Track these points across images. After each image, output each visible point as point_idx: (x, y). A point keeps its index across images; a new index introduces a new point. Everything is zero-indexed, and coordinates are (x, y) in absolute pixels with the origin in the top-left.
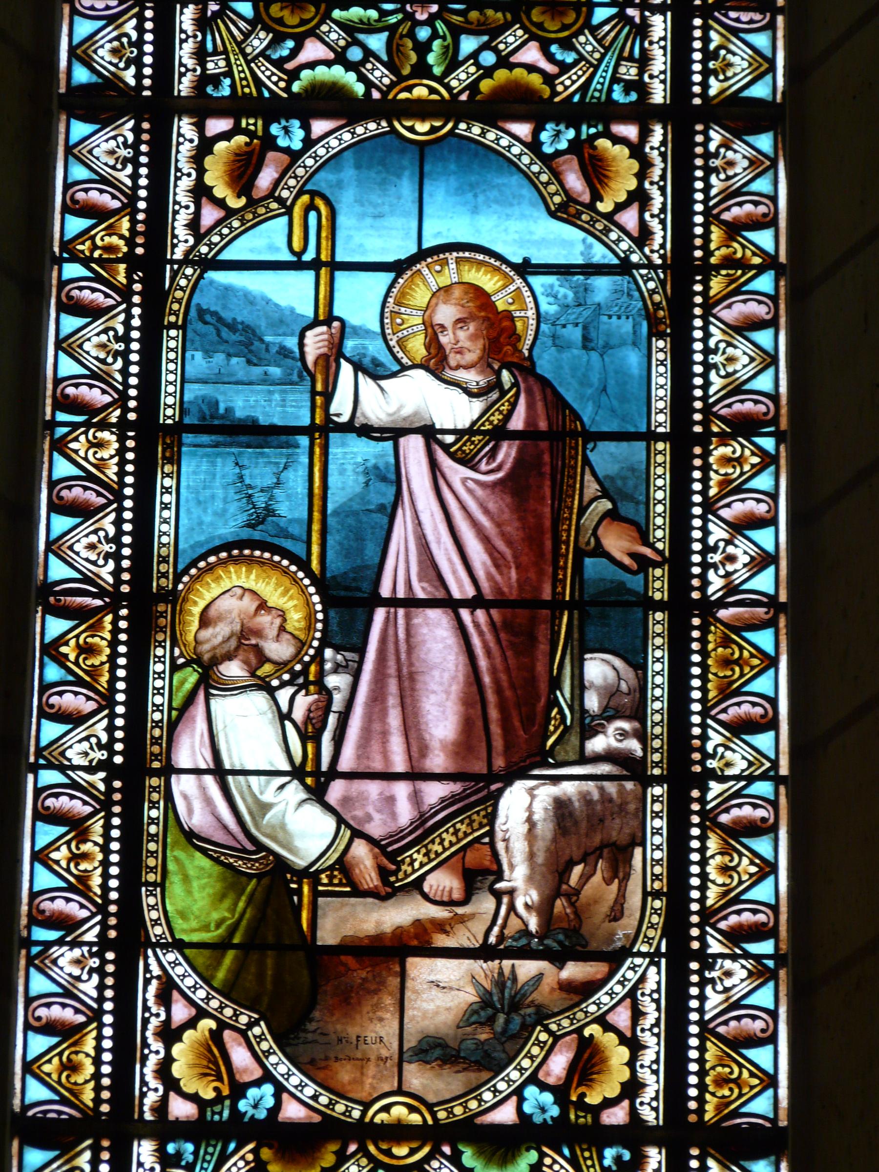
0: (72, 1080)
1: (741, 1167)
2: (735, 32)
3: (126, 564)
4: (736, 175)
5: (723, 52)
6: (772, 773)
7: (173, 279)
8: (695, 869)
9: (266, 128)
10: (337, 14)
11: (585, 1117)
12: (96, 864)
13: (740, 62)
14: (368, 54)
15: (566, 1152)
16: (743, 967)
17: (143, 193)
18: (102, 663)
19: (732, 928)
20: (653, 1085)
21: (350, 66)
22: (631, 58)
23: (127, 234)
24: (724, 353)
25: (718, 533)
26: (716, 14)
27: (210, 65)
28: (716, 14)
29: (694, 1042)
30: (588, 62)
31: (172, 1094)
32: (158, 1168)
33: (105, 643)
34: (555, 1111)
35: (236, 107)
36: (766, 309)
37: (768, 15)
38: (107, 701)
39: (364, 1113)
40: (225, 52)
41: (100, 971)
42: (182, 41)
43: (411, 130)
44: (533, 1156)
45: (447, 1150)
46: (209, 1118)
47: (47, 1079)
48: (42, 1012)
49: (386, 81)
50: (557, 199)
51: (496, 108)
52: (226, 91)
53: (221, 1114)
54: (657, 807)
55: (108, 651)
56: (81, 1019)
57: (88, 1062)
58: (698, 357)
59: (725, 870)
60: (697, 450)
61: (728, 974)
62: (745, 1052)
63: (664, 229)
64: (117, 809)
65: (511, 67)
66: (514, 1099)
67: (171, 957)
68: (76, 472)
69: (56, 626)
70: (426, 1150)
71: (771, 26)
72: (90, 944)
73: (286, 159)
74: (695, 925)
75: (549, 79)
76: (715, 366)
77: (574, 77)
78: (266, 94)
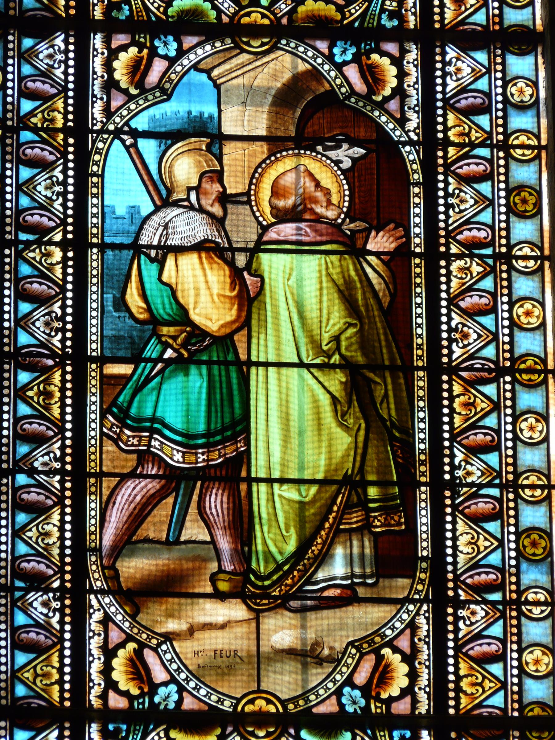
0: (46, 542)
3: (69, 335)
4: (469, 344)
6: (489, 142)
7: (94, 142)
8: (449, 543)
11: (381, 708)
16: (482, 609)
18: (54, 543)
19: (466, 240)
20: (97, 64)
24: (455, 65)
29: (444, 311)
35: (390, 722)
38: (60, 502)
42: (90, 638)
45: (292, 731)
49: (232, 10)
50: (164, 647)
53: (143, 703)
54: (418, 280)
55: (58, 534)
56: (54, 91)
57: (54, 671)
59: (466, 405)
61: (473, 613)
62: (487, 667)
64: (70, 263)
67: (107, 600)
68: (35, 342)
69: (24, 377)
70: (239, 708)
72: (54, 591)
73: (166, 64)
76: (450, 74)
77: (357, 8)
78: (154, 19)
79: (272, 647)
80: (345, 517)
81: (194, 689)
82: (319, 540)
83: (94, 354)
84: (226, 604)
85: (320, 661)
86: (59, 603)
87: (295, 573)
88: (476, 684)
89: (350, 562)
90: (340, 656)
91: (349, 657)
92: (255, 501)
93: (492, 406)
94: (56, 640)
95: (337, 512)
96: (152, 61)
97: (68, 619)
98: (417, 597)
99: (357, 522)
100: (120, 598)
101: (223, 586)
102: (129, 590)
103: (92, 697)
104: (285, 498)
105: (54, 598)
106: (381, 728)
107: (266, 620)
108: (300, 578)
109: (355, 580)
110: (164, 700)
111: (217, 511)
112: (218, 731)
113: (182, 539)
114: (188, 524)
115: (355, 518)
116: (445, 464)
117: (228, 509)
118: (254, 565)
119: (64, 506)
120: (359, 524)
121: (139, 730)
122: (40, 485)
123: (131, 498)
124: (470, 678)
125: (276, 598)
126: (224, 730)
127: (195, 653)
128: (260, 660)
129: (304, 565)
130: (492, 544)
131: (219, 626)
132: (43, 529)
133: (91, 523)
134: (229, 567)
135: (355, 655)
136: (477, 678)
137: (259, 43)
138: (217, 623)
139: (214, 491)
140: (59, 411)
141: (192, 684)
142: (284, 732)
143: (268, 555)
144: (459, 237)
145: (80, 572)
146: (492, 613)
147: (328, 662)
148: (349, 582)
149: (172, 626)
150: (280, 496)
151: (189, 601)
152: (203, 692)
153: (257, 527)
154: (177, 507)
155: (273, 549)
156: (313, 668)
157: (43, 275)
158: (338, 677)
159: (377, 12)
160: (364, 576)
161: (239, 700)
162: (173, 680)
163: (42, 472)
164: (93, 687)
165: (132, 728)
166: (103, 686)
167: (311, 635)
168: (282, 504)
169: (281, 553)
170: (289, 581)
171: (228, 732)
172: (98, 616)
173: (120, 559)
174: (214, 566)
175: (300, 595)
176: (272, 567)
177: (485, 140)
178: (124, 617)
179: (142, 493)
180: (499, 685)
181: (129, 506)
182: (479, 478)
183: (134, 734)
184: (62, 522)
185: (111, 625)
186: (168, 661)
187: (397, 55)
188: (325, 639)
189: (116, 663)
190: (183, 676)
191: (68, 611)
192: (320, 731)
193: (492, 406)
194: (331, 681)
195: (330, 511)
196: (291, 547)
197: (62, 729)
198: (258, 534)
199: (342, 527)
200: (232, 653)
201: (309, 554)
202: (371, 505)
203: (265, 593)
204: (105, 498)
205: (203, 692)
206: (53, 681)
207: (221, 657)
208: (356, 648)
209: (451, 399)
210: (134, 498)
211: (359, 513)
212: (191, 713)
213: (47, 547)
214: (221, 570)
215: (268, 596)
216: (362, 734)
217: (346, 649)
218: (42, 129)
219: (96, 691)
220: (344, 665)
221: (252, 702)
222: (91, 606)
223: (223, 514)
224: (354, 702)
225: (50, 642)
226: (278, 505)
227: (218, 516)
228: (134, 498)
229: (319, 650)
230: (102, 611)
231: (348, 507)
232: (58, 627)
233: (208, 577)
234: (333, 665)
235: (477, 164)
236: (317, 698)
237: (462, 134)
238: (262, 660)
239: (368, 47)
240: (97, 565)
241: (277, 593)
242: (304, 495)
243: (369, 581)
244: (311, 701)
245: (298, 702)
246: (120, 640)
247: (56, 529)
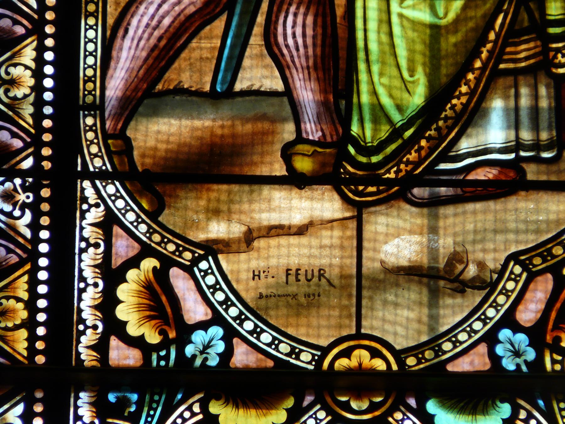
0: (11, 94)
15: (541, 403)
17: (44, 248)
18: (26, 96)
32: (97, 421)
33: (21, 305)
34: (531, 355)
38: (36, 28)
41: (34, 207)
42: (82, 251)
44: (506, 410)
45: (412, 402)
46: (155, 363)
50: (204, 265)
53: (167, 358)
67: (111, 189)
72: (23, 174)
79: (382, 262)
80: (508, 49)
81: (251, 333)
82: (464, 89)
84: (306, 192)
85: (461, 286)
86: (31, 195)
87: (423, 143)
89: (515, 122)
90: (495, 276)
91: (509, 279)
92: (359, 23)
94: (24, 256)
95: (495, 42)
96: (159, 222)
97: (45, 221)
99: (526, 58)
100: (131, 184)
101: (303, 165)
102: (146, 171)
103: (81, 349)
104: (408, 19)
105: (22, 186)
106: (560, 397)
107: (372, 218)
108: (431, 150)
109: (523, 154)
110: (202, 352)
111: (296, 43)
112: (290, 403)
113: (238, 87)
114: (246, 62)
115: (524, 51)
117: (314, 37)
118: (355, 129)
119: (43, 36)
120: (532, 61)
121: (158, 402)
123: (154, 23)
125: (390, 183)
126: (299, 401)
127: (256, 276)
128: (362, 284)
129: (438, 129)
131: (293, 230)
132: (7, 73)
133: (88, 64)
134: (315, 136)
135: (520, 275)
137: (365, 405)
138: (293, 224)
139: (292, 9)
141: (249, 325)
142: (399, 404)
143: (379, 113)
145: (68, 142)
147: (474, 288)
148: (512, 156)
149: (217, 230)
150: (401, 16)
151: (246, 188)
152: (266, 338)
153: (362, 66)
154: (231, 34)
155: (386, 100)
156: (450, 296)
158: (491, 312)
160: (537, 146)
161: (325, 351)
162: (217, 319)
164: (83, 333)
165: (147, 397)
166: (100, 330)
167: (446, 244)
168: (402, 26)
169: (400, 108)
170: (413, 156)
171: (305, 403)
172: (95, 215)
173: (132, 123)
174: (288, 132)
175: (431, 177)
176: (385, 131)
178: (138, 216)
179: (173, 14)
181: (151, 35)
183: (150, 408)
184: (40, 61)
185: (116, 230)
186: (209, 287)
188: (469, 248)
189: (124, 292)
190: (233, 312)
191: (45, 207)
192: (459, 402)
194: (479, 319)
195: (483, 41)
196: (418, 98)
197: (29, 403)
198: (363, 77)
199: (502, 66)
200: (316, 273)
201: (448, 108)
202: (552, 30)
203: (372, 175)
204: (110, 21)
205: (266, 338)
206: (18, 322)
207: (298, 280)
208: (522, 264)
210: (160, 22)
211: (532, 45)
212: (246, 372)
214: (300, 139)
215: (377, 181)
216: (528, 407)
217: (505, 266)
219: (89, 338)
220: (500, 293)
221: (347, 353)
222: (85, 200)
223: (305, 46)
224: (517, 354)
225: (14, 259)
226: (397, 30)
227: (297, 49)
228: (160, 22)
229: (460, 267)
230: (102, 207)
231: (512, 35)
232: (28, 233)
233: (278, 147)
234: (484, 293)
236: (455, 347)
238: (364, 283)
239: (163, 353)
240: (96, 132)
241: (392, 175)
242: (441, 14)
243: (546, 155)
244: (445, 353)
245: (423, 353)
246: (131, 254)
247: (29, 73)
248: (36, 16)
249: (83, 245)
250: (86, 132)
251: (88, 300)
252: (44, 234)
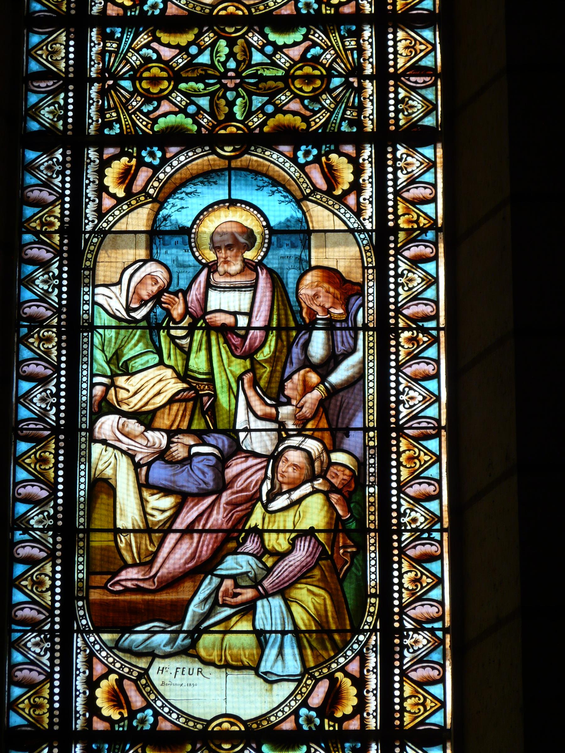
1: (423, 751)
2: (414, 89)
3: (63, 408)
5: (407, 99)
7: (86, 241)
9: (139, 153)
10: (183, 86)
11: (330, 10)
12: (46, 711)
13: (417, 104)
14: (261, 51)
15: (323, 745)
18: (50, 468)
20: (373, 704)
21: (273, 44)
22: (353, 107)
23: (59, 216)
24: (408, 394)
25: (403, 266)
26: (402, 78)
27: (353, 43)
28: (402, 78)
30: (327, 110)
31: (109, 4)
33: (47, 578)
36: (436, 672)
37: (433, 78)
38: (50, 677)
39: (212, 11)
40: (346, 50)
43: (232, 724)
45: (254, 745)
47: (39, 58)
48: (22, 491)
49: (250, 34)
51: (271, 140)
52: (118, 131)
53: (123, 726)
56: (42, 617)
58: (392, 280)
60: (392, 238)
62: (425, 565)
63: (372, 48)
65: (285, 113)
66: (293, 717)
68: (35, 297)
71: (435, 84)
74: (395, 518)
75: (305, 119)
77: (142, 40)
83: (82, 527)
88: (417, 704)
93: (436, 580)
98: (367, 627)
112: (196, 31)
116: (395, 599)
121: (131, 32)
122: (35, 540)
124: (413, 699)
130: (436, 704)
136: (419, 699)
137: (231, 148)
140: (50, 598)
144: (406, 253)
146: (428, 398)
157: (34, 602)
159: (338, 121)
163: (38, 529)
166: (97, 182)
177: (432, 225)
180: (439, 705)
182: (422, 523)
185: (95, 660)
187: (354, 155)
189: (355, 701)
193: (436, 580)
209: (399, 454)
212: (175, 17)
213: (48, 352)
218: (41, 232)
225: (42, 617)
235: (429, 484)
237: (410, 222)
246: (104, 672)
248: (61, 82)
249: (87, 182)
250: (84, 278)
251: (80, 703)
252: (57, 669)
